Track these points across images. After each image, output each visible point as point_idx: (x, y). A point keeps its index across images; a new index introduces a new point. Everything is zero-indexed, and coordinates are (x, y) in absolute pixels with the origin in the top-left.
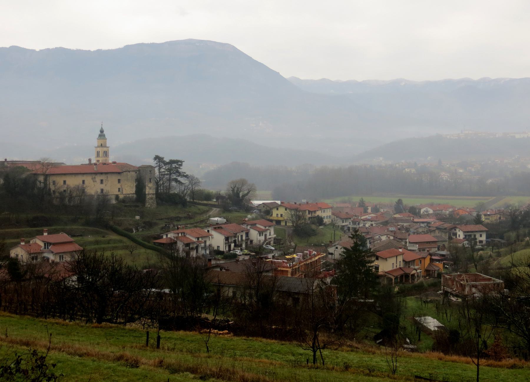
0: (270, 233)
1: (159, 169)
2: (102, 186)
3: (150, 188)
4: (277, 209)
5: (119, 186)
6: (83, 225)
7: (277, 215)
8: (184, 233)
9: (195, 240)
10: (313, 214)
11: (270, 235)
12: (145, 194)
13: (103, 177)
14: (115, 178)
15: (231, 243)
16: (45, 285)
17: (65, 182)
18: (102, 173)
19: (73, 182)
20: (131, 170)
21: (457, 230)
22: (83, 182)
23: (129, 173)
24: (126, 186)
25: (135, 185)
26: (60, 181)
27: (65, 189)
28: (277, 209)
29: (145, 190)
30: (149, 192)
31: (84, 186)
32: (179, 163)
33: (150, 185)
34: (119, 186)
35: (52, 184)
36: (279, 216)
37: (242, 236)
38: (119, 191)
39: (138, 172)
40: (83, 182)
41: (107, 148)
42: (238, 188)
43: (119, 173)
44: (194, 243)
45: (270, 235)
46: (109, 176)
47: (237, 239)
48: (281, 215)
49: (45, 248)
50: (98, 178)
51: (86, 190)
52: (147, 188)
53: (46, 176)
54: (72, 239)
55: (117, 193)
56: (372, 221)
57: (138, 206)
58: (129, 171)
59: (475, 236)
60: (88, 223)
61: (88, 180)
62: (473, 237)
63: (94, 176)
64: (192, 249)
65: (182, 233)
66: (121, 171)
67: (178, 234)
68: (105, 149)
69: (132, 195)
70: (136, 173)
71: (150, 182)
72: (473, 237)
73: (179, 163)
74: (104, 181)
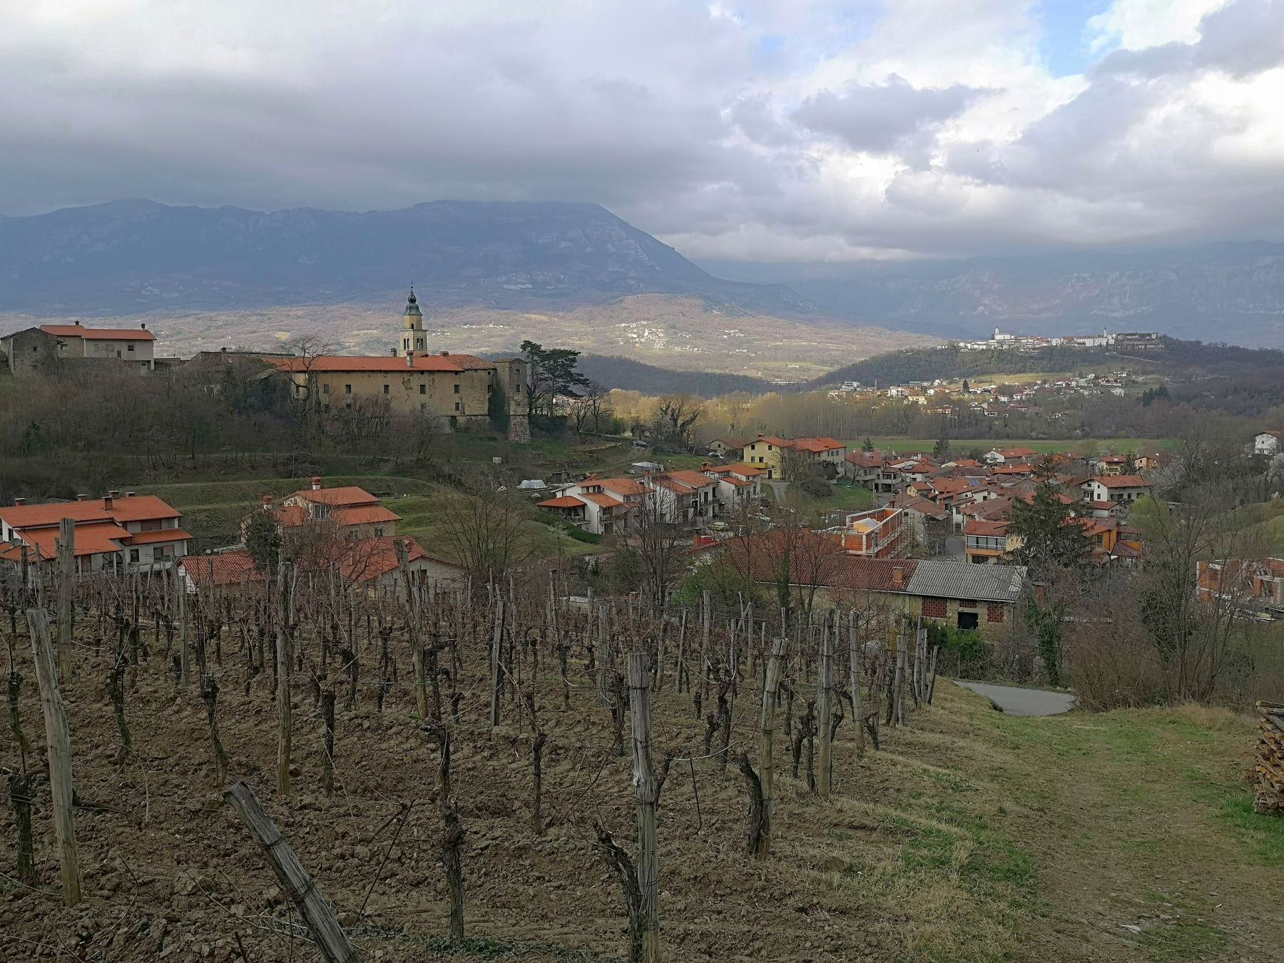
0: (755, 490)
1: (533, 367)
2: (424, 398)
3: (518, 404)
4: (753, 448)
5: (456, 398)
6: (393, 474)
7: (753, 459)
8: (599, 487)
9: (620, 499)
10: (817, 458)
11: (755, 494)
12: (508, 416)
13: (425, 379)
14: (450, 382)
15: (689, 507)
16: (626, 439)
17: (349, 387)
18: (422, 372)
19: (366, 388)
20: (479, 367)
21: (1095, 485)
22: (386, 387)
23: (475, 374)
24: (471, 398)
25: (488, 397)
26: (338, 383)
27: (349, 401)
28: (753, 448)
29: (509, 406)
30: (515, 411)
31: (389, 397)
32: (570, 357)
33: (518, 397)
34: (456, 398)
35: (321, 390)
36: (757, 460)
37: (706, 494)
38: (457, 408)
39: (492, 372)
40: (386, 387)
41: (424, 333)
42: (673, 410)
43: (456, 372)
44: (619, 505)
45: (755, 494)
46: (436, 376)
47: (698, 499)
48: (761, 459)
49: (317, 515)
50: (416, 381)
51: (393, 404)
52: (512, 403)
53: (312, 373)
54: (375, 499)
55: (454, 413)
56: (914, 474)
57: (494, 439)
58: (476, 370)
59: (1129, 496)
60: (400, 470)
61: (395, 383)
62: (1125, 497)
63: (406, 376)
64: (617, 518)
65: (594, 487)
66: (460, 369)
67: (588, 488)
68: (420, 334)
69: (483, 418)
70: (489, 373)
71: (518, 390)
72: (1125, 497)
73: (570, 357)
74: (427, 388)
